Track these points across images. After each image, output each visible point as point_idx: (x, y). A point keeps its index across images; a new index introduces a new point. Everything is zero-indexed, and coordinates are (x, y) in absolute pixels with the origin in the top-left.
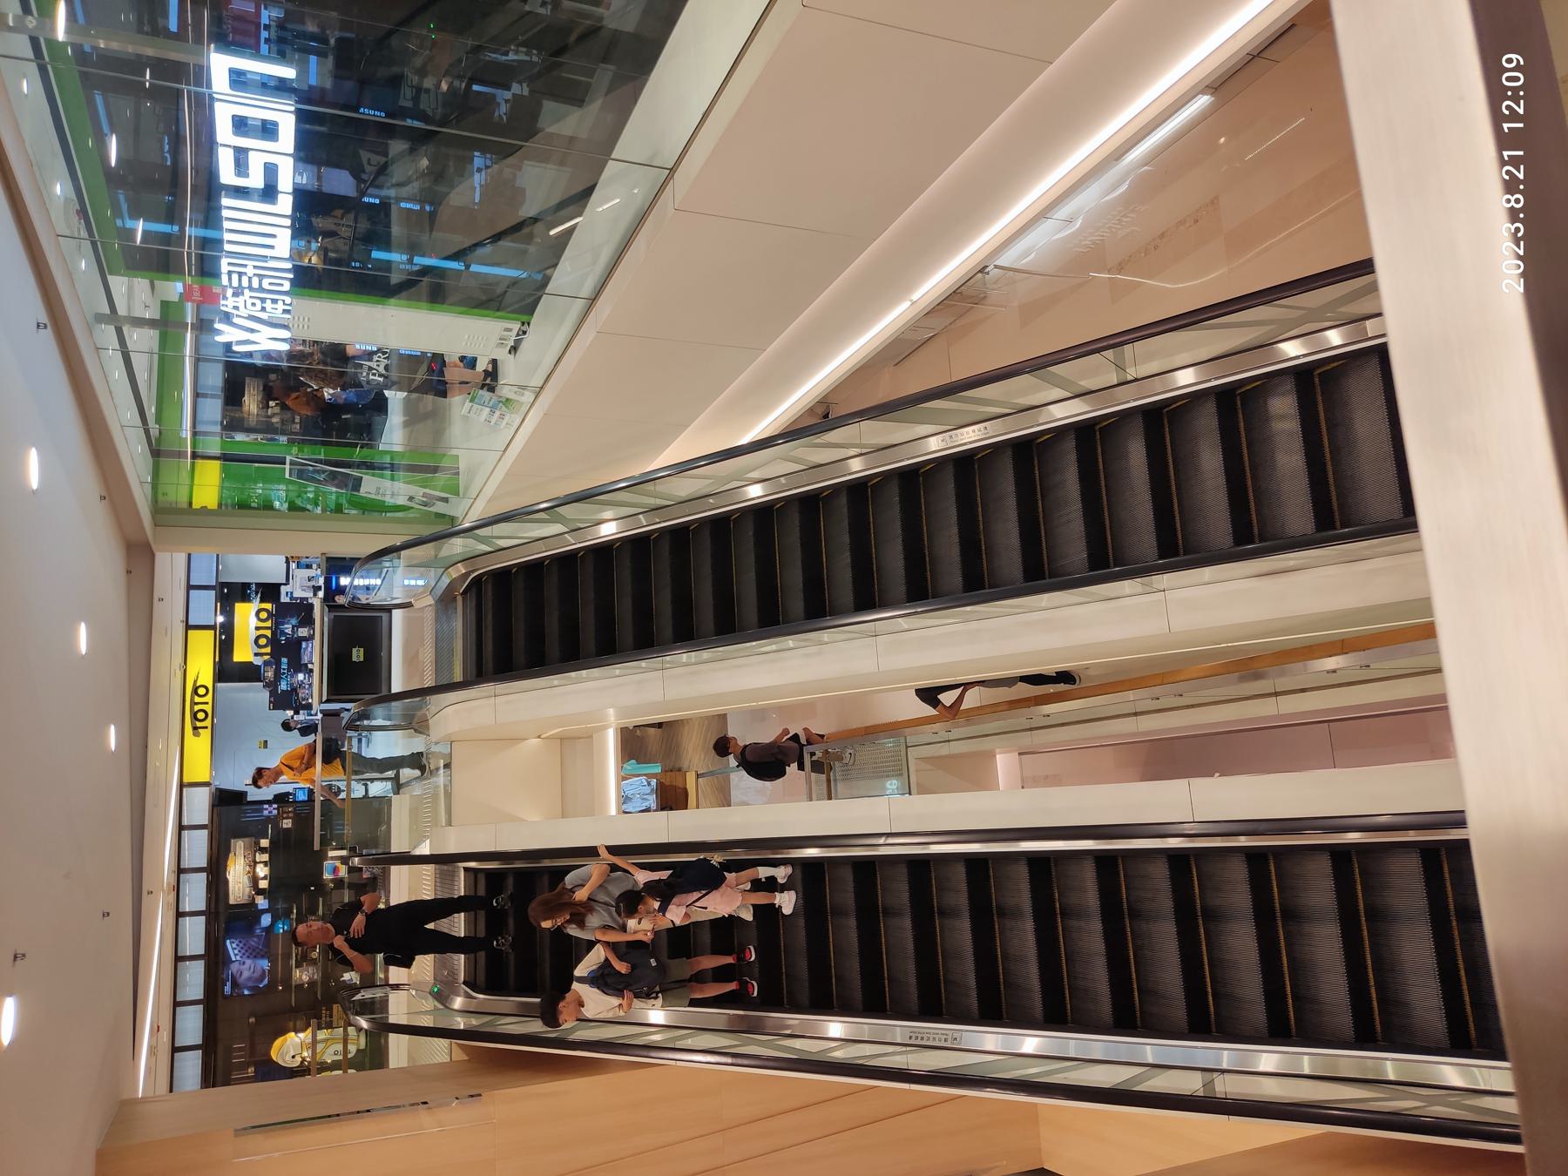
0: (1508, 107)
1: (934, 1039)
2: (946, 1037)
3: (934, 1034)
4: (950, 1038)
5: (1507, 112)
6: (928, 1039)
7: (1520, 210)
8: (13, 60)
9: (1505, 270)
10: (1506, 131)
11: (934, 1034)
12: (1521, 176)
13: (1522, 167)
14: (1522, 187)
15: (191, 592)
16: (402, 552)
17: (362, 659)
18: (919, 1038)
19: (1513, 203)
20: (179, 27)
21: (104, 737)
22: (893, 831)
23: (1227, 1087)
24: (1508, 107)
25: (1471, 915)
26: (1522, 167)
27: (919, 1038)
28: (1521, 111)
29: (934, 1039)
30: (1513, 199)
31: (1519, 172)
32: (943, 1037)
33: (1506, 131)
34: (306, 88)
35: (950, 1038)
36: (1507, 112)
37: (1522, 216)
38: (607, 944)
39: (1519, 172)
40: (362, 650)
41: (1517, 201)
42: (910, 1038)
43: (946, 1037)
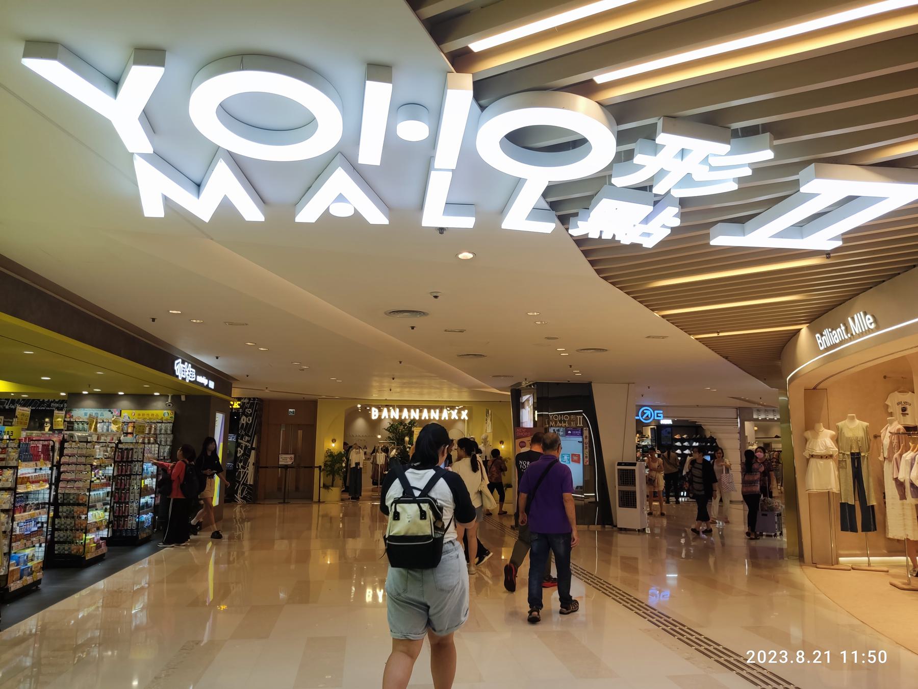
0: (817, 654)
5: (814, 653)
7: (795, 661)
8: (887, 354)
9: (760, 652)
10: (842, 653)
12: (815, 661)
13: (820, 662)
14: (809, 662)
19: (802, 656)
20: (255, 481)
21: (63, 392)
22: (433, 174)
24: (817, 654)
26: (820, 662)
28: (770, 662)
30: (799, 657)
31: (772, 661)
33: (842, 653)
34: (459, 448)
36: (814, 653)
37: (792, 662)
38: (239, 165)
39: (772, 661)
41: (800, 659)
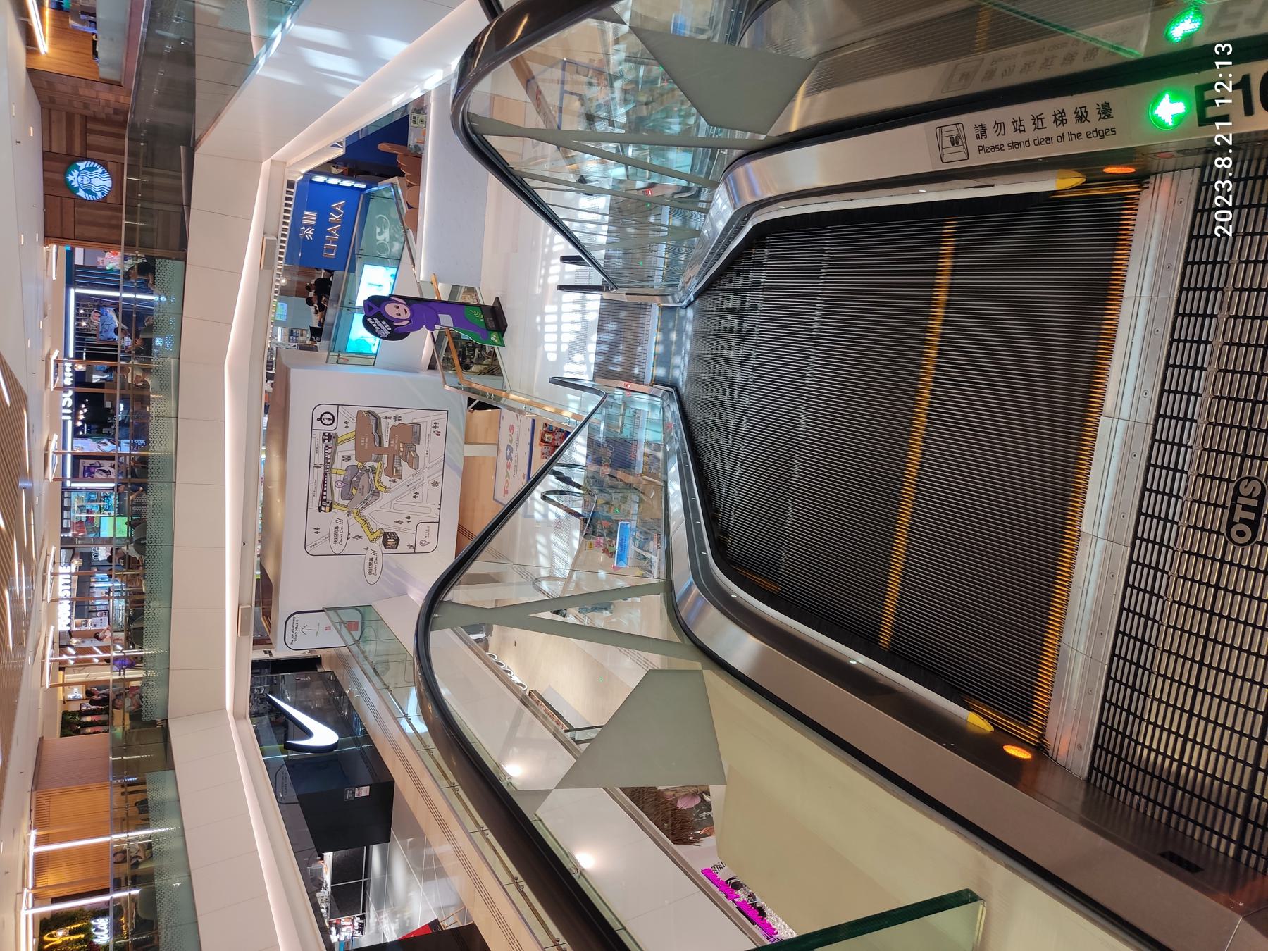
1: (1019, 127)
2: (983, 142)
3: (1026, 143)
4: (973, 143)
6: (981, 131)
11: (1026, 143)
15: (565, 95)
16: (493, 606)
17: (315, 214)
18: (1070, 117)
23: (918, 133)
25: (1244, 98)
27: (1070, 117)
29: (1019, 127)
30: (1223, 161)
32: (992, 139)
35: (973, 143)
40: (306, 213)
41: (1227, 163)
42: (1105, 111)
43: (983, 142)
